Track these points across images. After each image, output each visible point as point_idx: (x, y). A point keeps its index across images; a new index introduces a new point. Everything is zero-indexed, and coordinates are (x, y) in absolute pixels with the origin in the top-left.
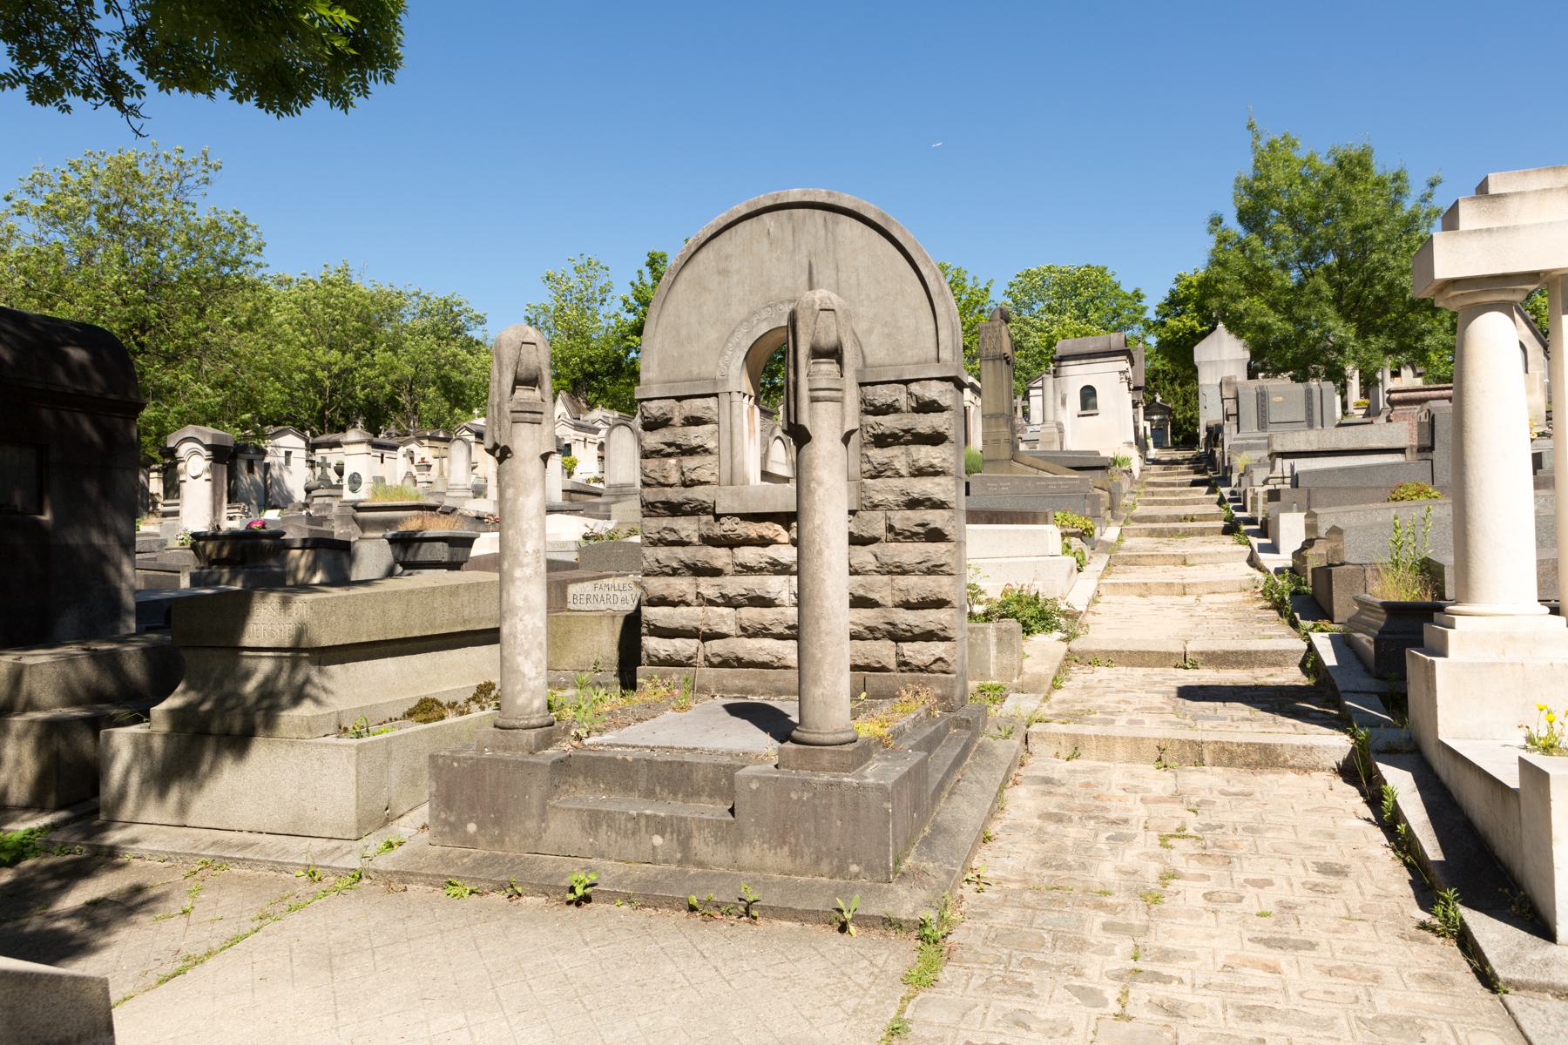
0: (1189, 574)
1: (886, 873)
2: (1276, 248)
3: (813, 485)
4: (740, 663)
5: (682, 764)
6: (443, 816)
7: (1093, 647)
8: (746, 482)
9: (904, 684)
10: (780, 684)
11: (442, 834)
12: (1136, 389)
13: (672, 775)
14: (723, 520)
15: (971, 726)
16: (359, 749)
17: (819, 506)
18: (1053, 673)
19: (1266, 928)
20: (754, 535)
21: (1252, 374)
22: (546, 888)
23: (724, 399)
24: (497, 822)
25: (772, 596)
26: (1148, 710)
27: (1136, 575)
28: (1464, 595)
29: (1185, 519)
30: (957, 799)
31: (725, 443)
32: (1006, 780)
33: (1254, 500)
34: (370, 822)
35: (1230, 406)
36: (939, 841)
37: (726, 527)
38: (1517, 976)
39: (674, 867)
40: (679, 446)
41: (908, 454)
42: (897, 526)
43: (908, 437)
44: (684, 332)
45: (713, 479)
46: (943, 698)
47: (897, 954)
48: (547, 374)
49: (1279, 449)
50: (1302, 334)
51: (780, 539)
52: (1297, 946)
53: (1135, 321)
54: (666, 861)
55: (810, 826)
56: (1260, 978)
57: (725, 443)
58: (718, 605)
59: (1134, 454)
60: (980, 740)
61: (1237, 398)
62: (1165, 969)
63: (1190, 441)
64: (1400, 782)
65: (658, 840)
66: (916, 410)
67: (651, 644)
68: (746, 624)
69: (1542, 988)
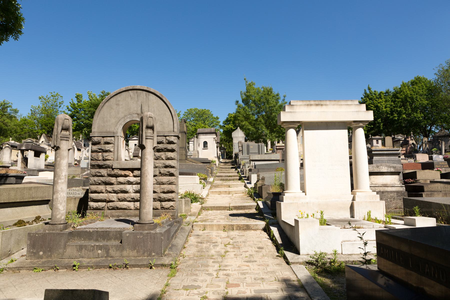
0: (231, 189)
1: (161, 254)
2: (252, 110)
3: (145, 159)
4: (118, 208)
5: (106, 231)
6: (32, 250)
7: (208, 206)
8: (121, 160)
9: (162, 213)
10: (129, 214)
11: (30, 256)
12: (218, 143)
13: (104, 235)
15: (180, 222)
16: (3, 233)
17: (147, 165)
18: (198, 211)
19: (247, 259)
20: (123, 174)
21: (246, 141)
22: (66, 267)
23: (116, 138)
24: (50, 251)
25: (128, 190)
26: (222, 219)
27: (217, 190)
28: (287, 189)
29: (229, 176)
30: (177, 239)
31: (116, 150)
32: (188, 235)
33: (246, 172)
34: (4, 255)
35: (241, 148)
36: (173, 248)
37: (115, 172)
38: (293, 261)
39: (104, 258)
41: (165, 154)
42: (162, 172)
43: (166, 150)
44: (105, 119)
45: (112, 159)
46: (172, 216)
47: (165, 272)
48: (71, 128)
49: (251, 159)
50: (257, 131)
51: (130, 175)
52: (253, 262)
53: (217, 125)
54: (102, 257)
55: (142, 244)
56: (246, 268)
57: (116, 150)
58: (112, 193)
59: (217, 160)
60: (181, 226)
61: (242, 146)
62: (226, 268)
63: (230, 157)
64: (274, 230)
65: (100, 252)
66: (168, 143)
67: (91, 204)
68: (120, 198)
69: (297, 263)
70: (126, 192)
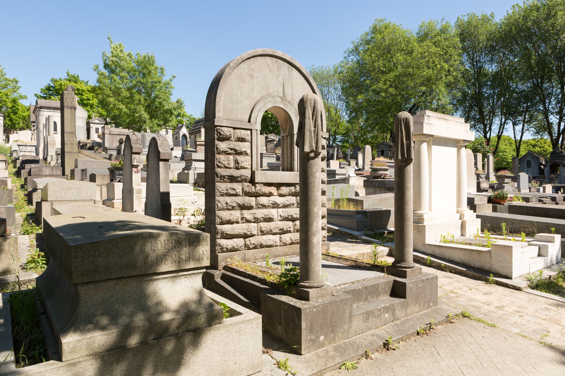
4: (262, 246)
6: (309, 338)
10: (276, 253)
14: (257, 185)
20: (267, 192)
24: (333, 331)
40: (235, 150)
65: (387, 315)
68: (263, 229)
70: (269, 220)
